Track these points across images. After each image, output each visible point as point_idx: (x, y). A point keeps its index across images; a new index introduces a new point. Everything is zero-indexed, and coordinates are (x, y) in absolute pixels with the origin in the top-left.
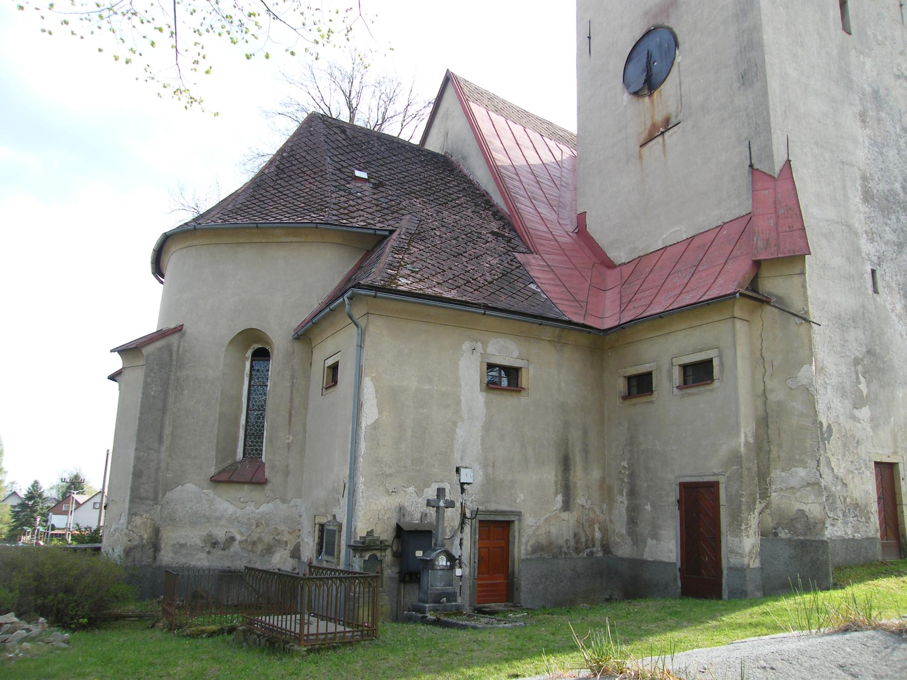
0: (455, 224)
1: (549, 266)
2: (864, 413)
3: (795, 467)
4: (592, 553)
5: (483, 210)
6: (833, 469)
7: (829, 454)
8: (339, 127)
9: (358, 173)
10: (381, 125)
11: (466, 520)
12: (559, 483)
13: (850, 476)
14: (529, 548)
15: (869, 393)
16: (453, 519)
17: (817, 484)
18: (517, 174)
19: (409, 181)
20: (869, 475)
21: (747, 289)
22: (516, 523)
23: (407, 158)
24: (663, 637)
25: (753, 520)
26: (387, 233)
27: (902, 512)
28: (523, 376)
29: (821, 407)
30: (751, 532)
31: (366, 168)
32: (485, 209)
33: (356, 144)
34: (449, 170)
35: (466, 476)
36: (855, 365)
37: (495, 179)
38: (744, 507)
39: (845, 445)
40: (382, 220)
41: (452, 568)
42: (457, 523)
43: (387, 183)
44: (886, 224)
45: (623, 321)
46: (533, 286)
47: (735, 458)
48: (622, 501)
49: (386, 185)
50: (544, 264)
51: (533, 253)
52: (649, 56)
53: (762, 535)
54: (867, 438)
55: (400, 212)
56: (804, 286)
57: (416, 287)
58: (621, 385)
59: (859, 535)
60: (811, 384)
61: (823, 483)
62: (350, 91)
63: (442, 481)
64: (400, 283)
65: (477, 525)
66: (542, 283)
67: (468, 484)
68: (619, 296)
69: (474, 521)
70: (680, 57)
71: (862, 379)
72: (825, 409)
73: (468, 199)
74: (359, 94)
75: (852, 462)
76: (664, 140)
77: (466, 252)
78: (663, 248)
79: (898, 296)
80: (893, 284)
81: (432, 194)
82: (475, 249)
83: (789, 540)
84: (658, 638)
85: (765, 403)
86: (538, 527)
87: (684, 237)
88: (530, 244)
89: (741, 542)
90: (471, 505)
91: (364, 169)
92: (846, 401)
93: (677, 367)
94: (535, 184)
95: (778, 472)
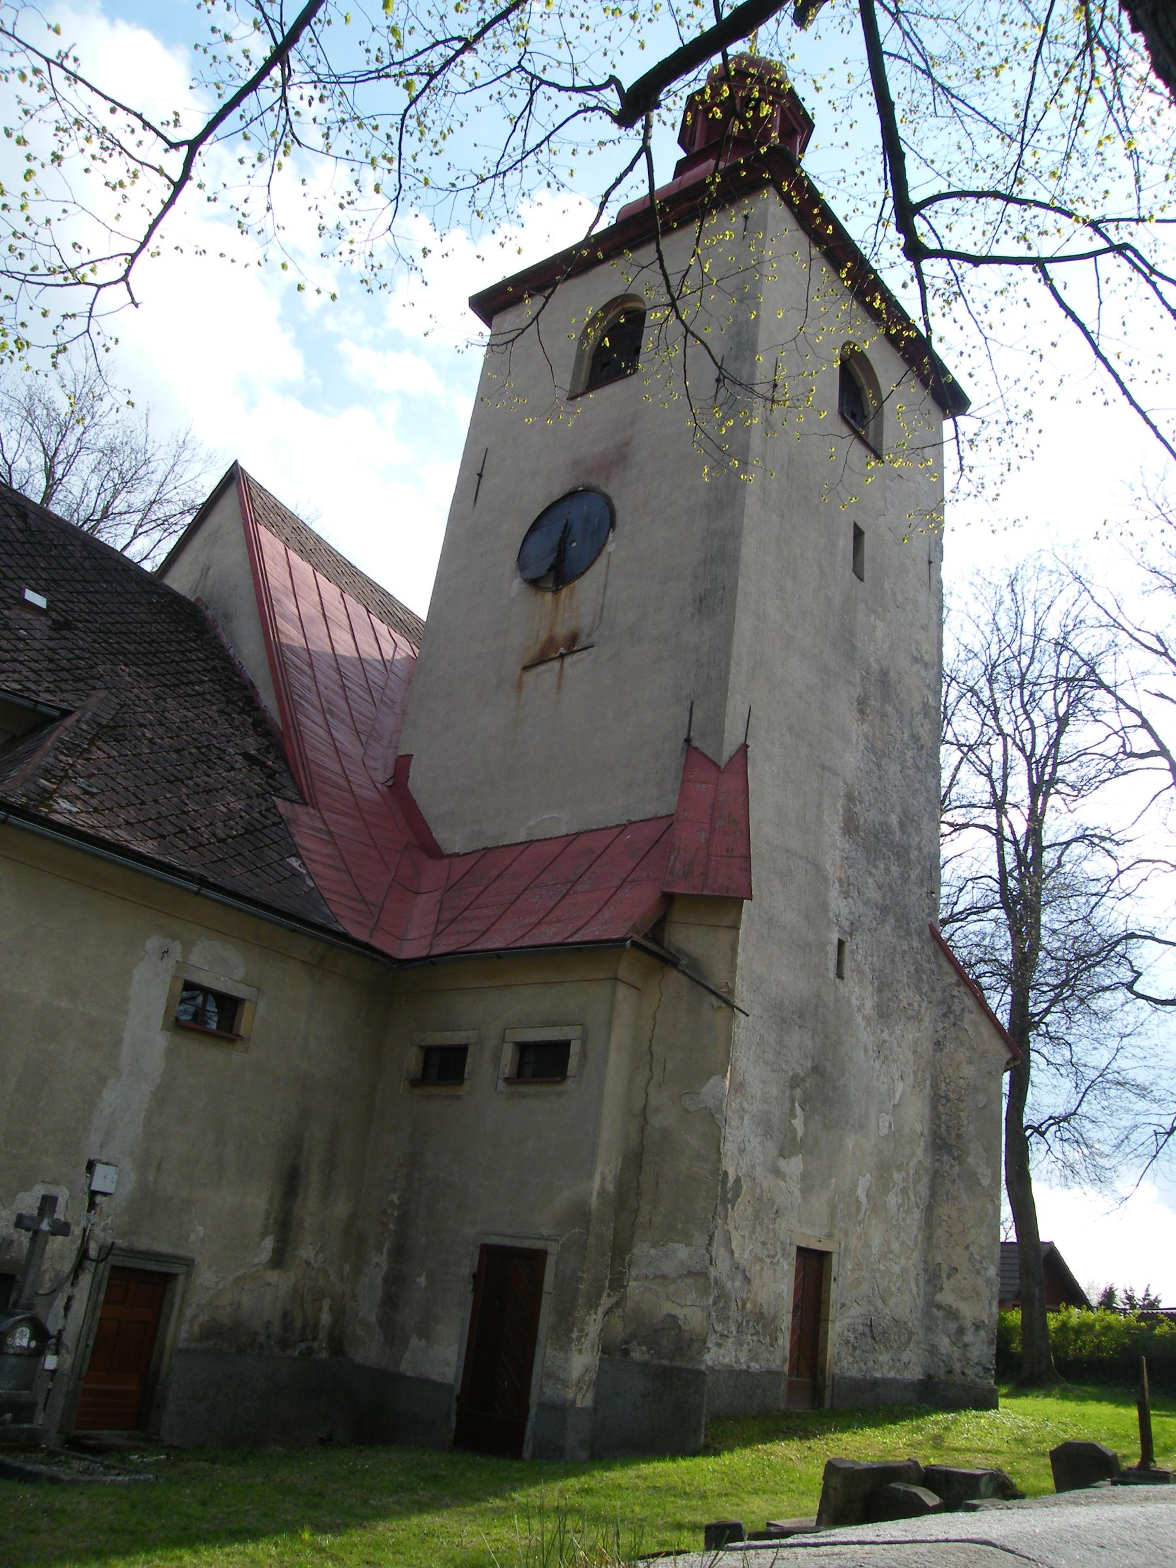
0: (184, 726)
1: (329, 832)
2: (794, 1166)
3: (674, 1241)
4: (309, 1352)
5: (239, 713)
6: (732, 1252)
7: (731, 1227)
8: (16, 505)
9: (31, 596)
10: (98, 521)
11: (87, 1263)
12: (273, 1215)
13: (758, 1268)
14: (196, 1329)
15: (806, 1134)
16: (61, 1258)
17: (704, 1274)
18: (311, 666)
19: (121, 632)
20: (786, 1267)
21: (645, 936)
22: (181, 1279)
23: (127, 592)
24: (404, 1523)
25: (594, 1324)
26: (57, 713)
27: (827, 1333)
28: (245, 1015)
29: (729, 1148)
30: (587, 1344)
31: (48, 590)
32: (242, 712)
33: (40, 543)
34: (195, 631)
35: (103, 1179)
36: (792, 1087)
37: (272, 666)
38: (580, 1301)
39: (757, 1216)
40: (53, 688)
41: (37, 1354)
42: (67, 1266)
43: (80, 625)
44: (870, 874)
45: (437, 951)
46: (294, 862)
47: (580, 1215)
48: (379, 1262)
49: (77, 628)
50: (324, 828)
51: (307, 804)
52: (567, 530)
53: (603, 1352)
54: (792, 1208)
55: (90, 681)
56: (734, 949)
57: (85, 822)
58: (412, 1060)
59: (757, 1366)
60: (719, 1109)
61: (713, 1273)
62: (57, 449)
63: (55, 1182)
64: (56, 807)
65: (107, 1274)
66: (311, 860)
67: (105, 1194)
68: (438, 907)
69: (101, 1266)
70: (614, 545)
71: (799, 1111)
72: (736, 1152)
73: (217, 687)
74: (71, 459)
75: (764, 1244)
76: (562, 668)
77: (190, 778)
78: (526, 842)
79: (870, 988)
80: (866, 968)
81: (155, 663)
82: (209, 776)
83: (645, 1365)
84: (394, 1525)
85: (643, 1128)
86: (220, 1291)
87: (564, 830)
88: (305, 787)
89: (567, 1360)
90: (102, 1235)
91: (44, 590)
92: (770, 1144)
93: (511, 1046)
94: (337, 689)
95: (645, 1246)
